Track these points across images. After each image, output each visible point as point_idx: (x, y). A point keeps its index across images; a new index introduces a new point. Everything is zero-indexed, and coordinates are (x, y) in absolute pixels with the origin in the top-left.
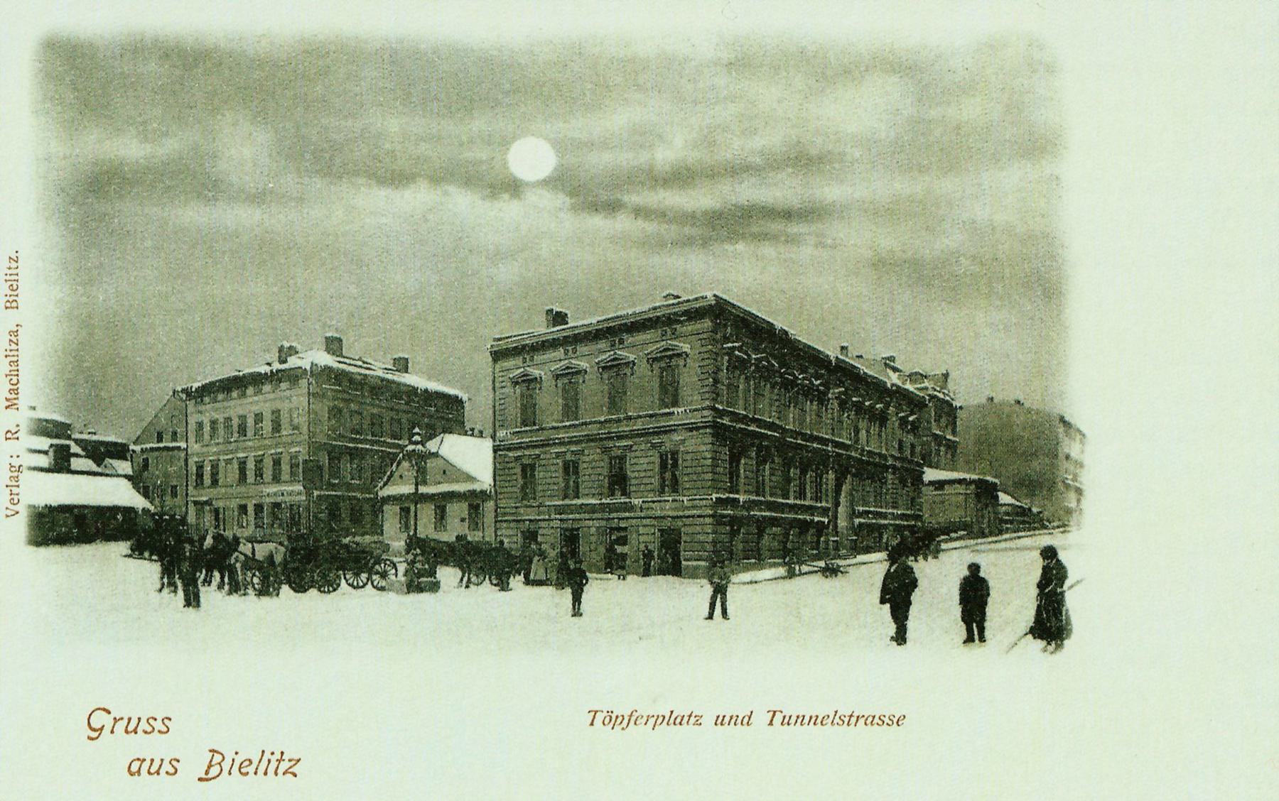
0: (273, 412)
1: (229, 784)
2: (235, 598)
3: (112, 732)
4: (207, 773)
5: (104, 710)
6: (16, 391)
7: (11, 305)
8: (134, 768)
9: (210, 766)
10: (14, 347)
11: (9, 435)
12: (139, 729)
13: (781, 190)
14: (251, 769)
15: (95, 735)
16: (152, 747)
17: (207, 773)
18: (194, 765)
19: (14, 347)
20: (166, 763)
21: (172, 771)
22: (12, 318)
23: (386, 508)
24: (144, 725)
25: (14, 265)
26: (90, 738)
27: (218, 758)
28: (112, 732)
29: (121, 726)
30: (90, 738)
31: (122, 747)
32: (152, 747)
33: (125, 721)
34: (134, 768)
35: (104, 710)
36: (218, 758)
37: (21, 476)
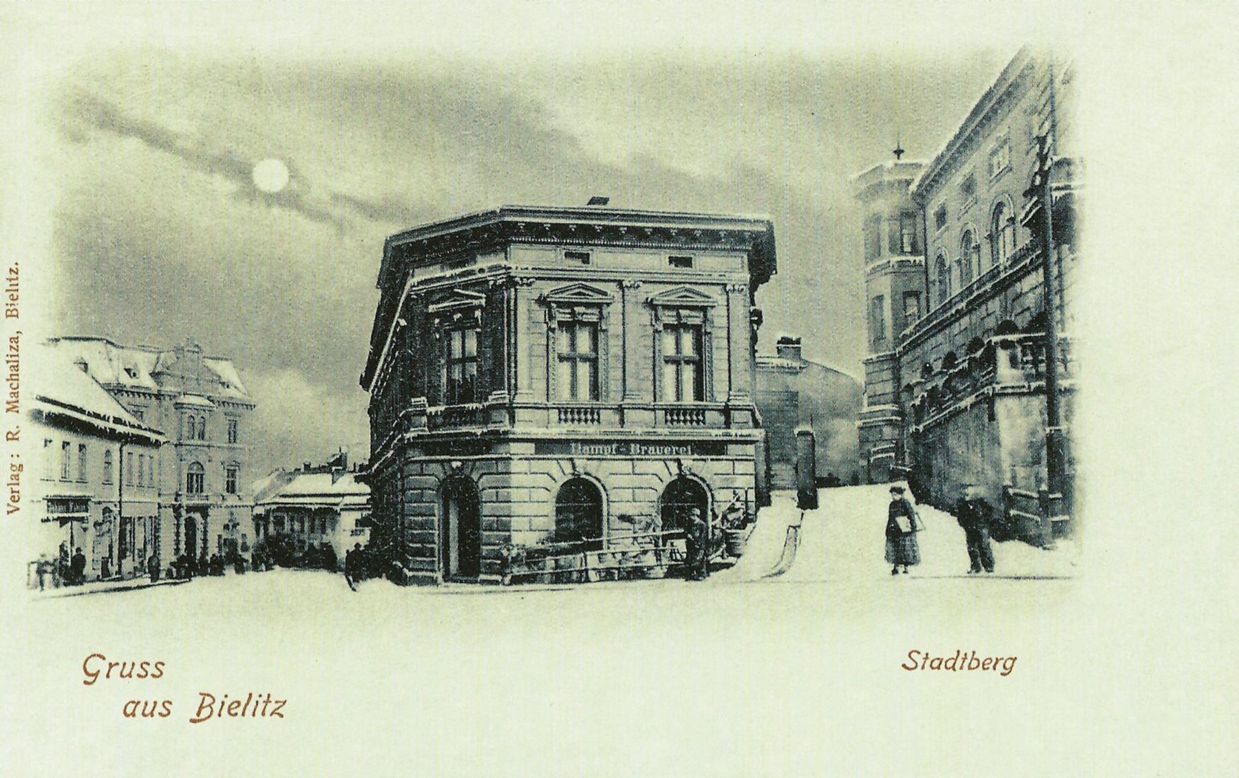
0: (670, 262)
1: (220, 725)
2: (240, 577)
3: (108, 676)
4: (198, 714)
5: (100, 656)
6: (15, 394)
7: (12, 313)
8: (129, 711)
9: (201, 707)
10: (14, 352)
11: (10, 436)
12: (156, 713)
13: (153, 437)
14: (239, 711)
15: (90, 679)
16: (147, 690)
17: (198, 714)
18: (186, 707)
19: (14, 352)
20: (137, 667)
21: (165, 712)
22: (11, 327)
23: (817, 475)
24: (138, 670)
25: (14, 276)
26: (86, 683)
27: (208, 700)
28: (108, 676)
29: (116, 671)
30: (86, 683)
31: (116, 691)
32: (147, 690)
33: (121, 666)
34: (129, 711)
35: (100, 656)
36: (208, 700)
37: (21, 474)
